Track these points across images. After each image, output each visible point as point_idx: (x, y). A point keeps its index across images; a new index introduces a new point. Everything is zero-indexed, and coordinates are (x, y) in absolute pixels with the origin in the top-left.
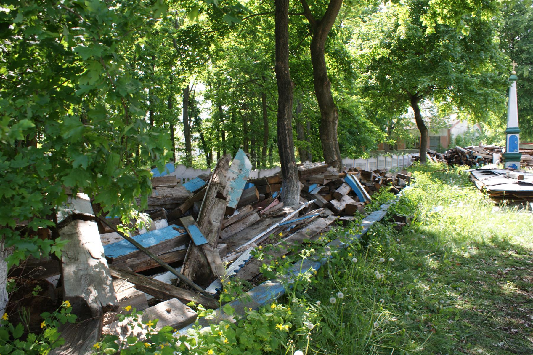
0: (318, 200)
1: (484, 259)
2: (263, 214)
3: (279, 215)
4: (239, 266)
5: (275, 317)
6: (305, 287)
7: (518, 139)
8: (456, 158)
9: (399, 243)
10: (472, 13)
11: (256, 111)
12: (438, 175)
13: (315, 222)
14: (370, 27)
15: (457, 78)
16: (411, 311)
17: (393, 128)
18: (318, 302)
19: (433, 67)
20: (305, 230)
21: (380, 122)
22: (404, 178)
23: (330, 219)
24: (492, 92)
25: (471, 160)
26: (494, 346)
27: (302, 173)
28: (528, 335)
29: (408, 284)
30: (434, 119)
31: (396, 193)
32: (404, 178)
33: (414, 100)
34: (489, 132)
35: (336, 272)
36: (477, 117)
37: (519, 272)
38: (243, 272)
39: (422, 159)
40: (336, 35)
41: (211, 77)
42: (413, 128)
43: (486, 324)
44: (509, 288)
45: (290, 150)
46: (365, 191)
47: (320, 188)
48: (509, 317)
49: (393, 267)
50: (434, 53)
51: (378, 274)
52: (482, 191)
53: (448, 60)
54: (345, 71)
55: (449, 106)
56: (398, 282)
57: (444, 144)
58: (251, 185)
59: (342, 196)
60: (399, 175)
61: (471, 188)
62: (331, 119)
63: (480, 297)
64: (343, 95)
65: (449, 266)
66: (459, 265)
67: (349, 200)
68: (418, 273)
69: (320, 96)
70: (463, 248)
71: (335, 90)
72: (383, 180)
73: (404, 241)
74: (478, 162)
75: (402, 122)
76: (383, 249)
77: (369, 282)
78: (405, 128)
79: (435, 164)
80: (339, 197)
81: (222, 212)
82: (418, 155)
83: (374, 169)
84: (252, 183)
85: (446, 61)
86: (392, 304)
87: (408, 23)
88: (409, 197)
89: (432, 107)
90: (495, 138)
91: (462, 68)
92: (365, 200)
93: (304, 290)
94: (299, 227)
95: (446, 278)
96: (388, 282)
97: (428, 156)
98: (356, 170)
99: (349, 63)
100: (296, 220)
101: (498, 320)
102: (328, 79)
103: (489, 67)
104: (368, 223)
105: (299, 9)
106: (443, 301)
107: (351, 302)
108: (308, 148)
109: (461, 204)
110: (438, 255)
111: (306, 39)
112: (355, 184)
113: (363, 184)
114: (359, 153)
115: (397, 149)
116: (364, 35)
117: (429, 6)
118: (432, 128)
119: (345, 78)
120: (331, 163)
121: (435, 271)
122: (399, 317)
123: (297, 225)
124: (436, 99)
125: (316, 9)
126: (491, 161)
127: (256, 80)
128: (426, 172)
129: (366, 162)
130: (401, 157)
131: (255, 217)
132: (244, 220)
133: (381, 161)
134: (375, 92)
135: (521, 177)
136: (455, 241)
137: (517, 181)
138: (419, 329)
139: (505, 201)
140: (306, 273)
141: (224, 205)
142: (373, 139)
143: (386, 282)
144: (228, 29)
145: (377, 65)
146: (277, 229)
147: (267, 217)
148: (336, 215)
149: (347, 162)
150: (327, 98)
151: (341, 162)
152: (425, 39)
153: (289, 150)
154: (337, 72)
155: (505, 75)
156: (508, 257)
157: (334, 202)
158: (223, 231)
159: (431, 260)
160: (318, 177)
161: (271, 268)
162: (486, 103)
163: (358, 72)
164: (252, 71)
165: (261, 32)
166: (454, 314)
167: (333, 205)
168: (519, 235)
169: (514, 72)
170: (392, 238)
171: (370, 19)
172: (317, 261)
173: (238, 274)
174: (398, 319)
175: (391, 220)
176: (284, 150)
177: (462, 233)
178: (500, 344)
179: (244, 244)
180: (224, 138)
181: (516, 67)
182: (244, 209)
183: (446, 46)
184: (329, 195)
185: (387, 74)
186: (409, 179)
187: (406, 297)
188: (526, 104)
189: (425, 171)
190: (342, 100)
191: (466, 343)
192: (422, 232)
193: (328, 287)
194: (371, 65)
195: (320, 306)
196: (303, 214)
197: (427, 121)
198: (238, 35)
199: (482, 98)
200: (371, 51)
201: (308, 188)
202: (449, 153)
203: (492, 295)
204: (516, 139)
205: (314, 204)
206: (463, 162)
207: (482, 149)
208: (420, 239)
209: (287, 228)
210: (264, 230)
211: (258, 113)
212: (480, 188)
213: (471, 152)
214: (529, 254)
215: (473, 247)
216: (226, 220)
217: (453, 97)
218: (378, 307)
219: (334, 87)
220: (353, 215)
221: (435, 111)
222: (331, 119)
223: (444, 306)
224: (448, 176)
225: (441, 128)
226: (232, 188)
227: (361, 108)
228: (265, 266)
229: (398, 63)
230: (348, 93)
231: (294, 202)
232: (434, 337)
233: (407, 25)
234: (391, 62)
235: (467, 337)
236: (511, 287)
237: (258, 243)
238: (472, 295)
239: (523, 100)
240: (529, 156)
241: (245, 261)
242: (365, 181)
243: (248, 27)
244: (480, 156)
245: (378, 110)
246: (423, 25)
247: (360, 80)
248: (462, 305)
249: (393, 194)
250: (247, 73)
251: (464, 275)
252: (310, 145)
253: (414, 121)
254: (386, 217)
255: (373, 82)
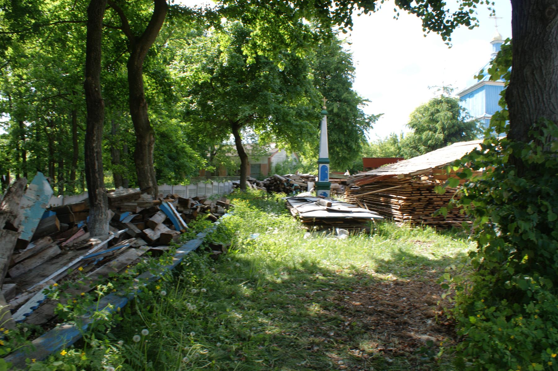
0: (130, 229)
1: (294, 283)
2: (66, 246)
3: (85, 246)
4: (31, 308)
5: (65, 365)
6: (108, 326)
7: (329, 169)
8: (274, 186)
9: (215, 272)
10: (289, 49)
11: (64, 130)
12: (258, 203)
13: (125, 254)
14: (194, 50)
15: (276, 109)
16: (222, 342)
17: (215, 154)
18: (121, 342)
19: (251, 97)
20: (114, 263)
21: (201, 149)
22: (223, 205)
23: (142, 250)
24: (306, 124)
25: (288, 188)
26: (299, 366)
27: (112, 200)
28: (327, 351)
29: (221, 314)
30: (255, 146)
31: (213, 220)
32: (223, 205)
33: (236, 128)
34: (305, 162)
35: (145, 307)
36: (293, 147)
37: (323, 293)
38: (35, 315)
39: (242, 186)
40: (156, 54)
41: (9, 86)
42: (235, 155)
43: (292, 345)
44: (315, 309)
45: (99, 175)
46: (181, 219)
47: (133, 216)
48: (313, 336)
49: (207, 297)
50: (255, 83)
51: (190, 306)
52: (296, 217)
53: (268, 91)
54: (165, 93)
55: (268, 135)
56: (210, 313)
57: (264, 172)
58: (52, 214)
59: (156, 224)
60: (218, 202)
61: (286, 215)
62: (147, 143)
63: (289, 321)
64: (162, 118)
65: (261, 293)
66: (272, 290)
67: (164, 229)
68: (231, 302)
69: (136, 119)
70: (276, 274)
71: (154, 112)
72: (202, 208)
73: (220, 270)
74: (295, 189)
75: (224, 148)
76: (198, 280)
77: (180, 315)
78: (227, 155)
79: (254, 191)
80: (153, 226)
81: (11, 246)
82: (238, 182)
83: (193, 196)
84: (53, 211)
85: (266, 92)
86: (203, 336)
87: (230, 51)
88: (227, 225)
89: (253, 135)
90: (310, 168)
91: (281, 100)
92: (181, 229)
93: (106, 330)
94: (107, 259)
95: (258, 305)
96: (201, 313)
97: (248, 183)
98: (173, 197)
99: (170, 85)
100: (103, 251)
101: (304, 341)
102: (145, 100)
103: (305, 100)
104: (182, 253)
105: (117, 23)
106: (255, 328)
107: (159, 338)
108: (123, 172)
109: (276, 232)
110: (252, 282)
111: (123, 55)
112: (171, 212)
113: (179, 212)
114: (179, 179)
115: (218, 175)
116: (187, 57)
117: (250, 37)
118: (253, 155)
119: (165, 100)
120: (146, 190)
121: (248, 298)
122: (210, 349)
123: (105, 258)
124: (256, 127)
125: (135, 25)
126: (306, 189)
127: (65, 95)
128: (245, 199)
129: (185, 189)
130: (221, 185)
131: (55, 250)
132: (41, 254)
133: (200, 188)
134: (196, 116)
135: (330, 205)
136: (269, 267)
137: (326, 208)
138: (229, 359)
139: (315, 227)
140: (103, 311)
141: (14, 238)
142: (192, 165)
143: (198, 313)
144: (30, 33)
145: (199, 89)
146: (81, 263)
147: (70, 250)
148: (148, 245)
149: (164, 188)
150: (144, 120)
151: (156, 189)
152: (248, 68)
153: (97, 175)
154: (156, 93)
155: (317, 110)
156: (315, 280)
157: (148, 231)
158: (13, 269)
159: (245, 287)
160: (130, 204)
161: (69, 308)
162: (301, 134)
163: (179, 94)
164: (61, 85)
165: (72, 42)
166: (264, 340)
167: (146, 235)
168: (325, 259)
169: (325, 107)
170: (207, 268)
171: (194, 43)
172: (124, 296)
173: (29, 318)
174: (210, 351)
175: (207, 249)
176: (91, 175)
177: (276, 259)
178: (303, 363)
179: (39, 282)
180: (24, 157)
181: (326, 102)
182: (41, 241)
183: (266, 77)
184: (142, 224)
185: (209, 99)
186: (227, 207)
187: (218, 328)
188: (335, 137)
189: (244, 199)
190: (159, 123)
191: (274, 367)
192: (239, 260)
193: (136, 324)
194: (193, 89)
195: (123, 346)
196: (113, 245)
197: (248, 148)
198: (44, 42)
199: (298, 129)
200: (192, 74)
201: (119, 217)
202: (268, 180)
203: (299, 318)
204: (327, 169)
205: (125, 233)
206: (281, 189)
207: (298, 178)
208: (235, 267)
209: (93, 261)
210: (65, 264)
211: (67, 132)
212: (294, 215)
213: (288, 180)
214: (333, 276)
215: (285, 273)
216: (17, 255)
217: (272, 127)
218: (189, 341)
219: (152, 109)
220: (169, 245)
221: (256, 139)
222: (147, 143)
223: (255, 333)
224: (267, 203)
225: (262, 156)
226: (26, 218)
227: (180, 133)
228: (60, 306)
229: (220, 90)
230: (167, 116)
231: (103, 232)
232: (243, 365)
233: (229, 51)
234: (213, 88)
235: (275, 361)
236: (316, 308)
237: (57, 279)
238: (282, 320)
239: (333, 133)
240: (338, 184)
241: (38, 302)
242: (182, 209)
243: (56, 34)
244: (297, 184)
245: (199, 136)
246: (244, 54)
247: (181, 104)
248: (273, 330)
249: (210, 222)
250: (54, 84)
251: (275, 301)
252: (126, 170)
253: (235, 148)
254: (202, 245)
255: (194, 106)
